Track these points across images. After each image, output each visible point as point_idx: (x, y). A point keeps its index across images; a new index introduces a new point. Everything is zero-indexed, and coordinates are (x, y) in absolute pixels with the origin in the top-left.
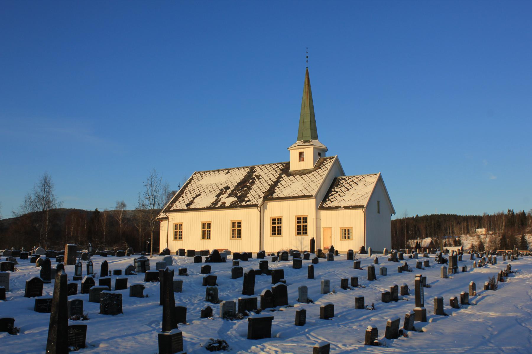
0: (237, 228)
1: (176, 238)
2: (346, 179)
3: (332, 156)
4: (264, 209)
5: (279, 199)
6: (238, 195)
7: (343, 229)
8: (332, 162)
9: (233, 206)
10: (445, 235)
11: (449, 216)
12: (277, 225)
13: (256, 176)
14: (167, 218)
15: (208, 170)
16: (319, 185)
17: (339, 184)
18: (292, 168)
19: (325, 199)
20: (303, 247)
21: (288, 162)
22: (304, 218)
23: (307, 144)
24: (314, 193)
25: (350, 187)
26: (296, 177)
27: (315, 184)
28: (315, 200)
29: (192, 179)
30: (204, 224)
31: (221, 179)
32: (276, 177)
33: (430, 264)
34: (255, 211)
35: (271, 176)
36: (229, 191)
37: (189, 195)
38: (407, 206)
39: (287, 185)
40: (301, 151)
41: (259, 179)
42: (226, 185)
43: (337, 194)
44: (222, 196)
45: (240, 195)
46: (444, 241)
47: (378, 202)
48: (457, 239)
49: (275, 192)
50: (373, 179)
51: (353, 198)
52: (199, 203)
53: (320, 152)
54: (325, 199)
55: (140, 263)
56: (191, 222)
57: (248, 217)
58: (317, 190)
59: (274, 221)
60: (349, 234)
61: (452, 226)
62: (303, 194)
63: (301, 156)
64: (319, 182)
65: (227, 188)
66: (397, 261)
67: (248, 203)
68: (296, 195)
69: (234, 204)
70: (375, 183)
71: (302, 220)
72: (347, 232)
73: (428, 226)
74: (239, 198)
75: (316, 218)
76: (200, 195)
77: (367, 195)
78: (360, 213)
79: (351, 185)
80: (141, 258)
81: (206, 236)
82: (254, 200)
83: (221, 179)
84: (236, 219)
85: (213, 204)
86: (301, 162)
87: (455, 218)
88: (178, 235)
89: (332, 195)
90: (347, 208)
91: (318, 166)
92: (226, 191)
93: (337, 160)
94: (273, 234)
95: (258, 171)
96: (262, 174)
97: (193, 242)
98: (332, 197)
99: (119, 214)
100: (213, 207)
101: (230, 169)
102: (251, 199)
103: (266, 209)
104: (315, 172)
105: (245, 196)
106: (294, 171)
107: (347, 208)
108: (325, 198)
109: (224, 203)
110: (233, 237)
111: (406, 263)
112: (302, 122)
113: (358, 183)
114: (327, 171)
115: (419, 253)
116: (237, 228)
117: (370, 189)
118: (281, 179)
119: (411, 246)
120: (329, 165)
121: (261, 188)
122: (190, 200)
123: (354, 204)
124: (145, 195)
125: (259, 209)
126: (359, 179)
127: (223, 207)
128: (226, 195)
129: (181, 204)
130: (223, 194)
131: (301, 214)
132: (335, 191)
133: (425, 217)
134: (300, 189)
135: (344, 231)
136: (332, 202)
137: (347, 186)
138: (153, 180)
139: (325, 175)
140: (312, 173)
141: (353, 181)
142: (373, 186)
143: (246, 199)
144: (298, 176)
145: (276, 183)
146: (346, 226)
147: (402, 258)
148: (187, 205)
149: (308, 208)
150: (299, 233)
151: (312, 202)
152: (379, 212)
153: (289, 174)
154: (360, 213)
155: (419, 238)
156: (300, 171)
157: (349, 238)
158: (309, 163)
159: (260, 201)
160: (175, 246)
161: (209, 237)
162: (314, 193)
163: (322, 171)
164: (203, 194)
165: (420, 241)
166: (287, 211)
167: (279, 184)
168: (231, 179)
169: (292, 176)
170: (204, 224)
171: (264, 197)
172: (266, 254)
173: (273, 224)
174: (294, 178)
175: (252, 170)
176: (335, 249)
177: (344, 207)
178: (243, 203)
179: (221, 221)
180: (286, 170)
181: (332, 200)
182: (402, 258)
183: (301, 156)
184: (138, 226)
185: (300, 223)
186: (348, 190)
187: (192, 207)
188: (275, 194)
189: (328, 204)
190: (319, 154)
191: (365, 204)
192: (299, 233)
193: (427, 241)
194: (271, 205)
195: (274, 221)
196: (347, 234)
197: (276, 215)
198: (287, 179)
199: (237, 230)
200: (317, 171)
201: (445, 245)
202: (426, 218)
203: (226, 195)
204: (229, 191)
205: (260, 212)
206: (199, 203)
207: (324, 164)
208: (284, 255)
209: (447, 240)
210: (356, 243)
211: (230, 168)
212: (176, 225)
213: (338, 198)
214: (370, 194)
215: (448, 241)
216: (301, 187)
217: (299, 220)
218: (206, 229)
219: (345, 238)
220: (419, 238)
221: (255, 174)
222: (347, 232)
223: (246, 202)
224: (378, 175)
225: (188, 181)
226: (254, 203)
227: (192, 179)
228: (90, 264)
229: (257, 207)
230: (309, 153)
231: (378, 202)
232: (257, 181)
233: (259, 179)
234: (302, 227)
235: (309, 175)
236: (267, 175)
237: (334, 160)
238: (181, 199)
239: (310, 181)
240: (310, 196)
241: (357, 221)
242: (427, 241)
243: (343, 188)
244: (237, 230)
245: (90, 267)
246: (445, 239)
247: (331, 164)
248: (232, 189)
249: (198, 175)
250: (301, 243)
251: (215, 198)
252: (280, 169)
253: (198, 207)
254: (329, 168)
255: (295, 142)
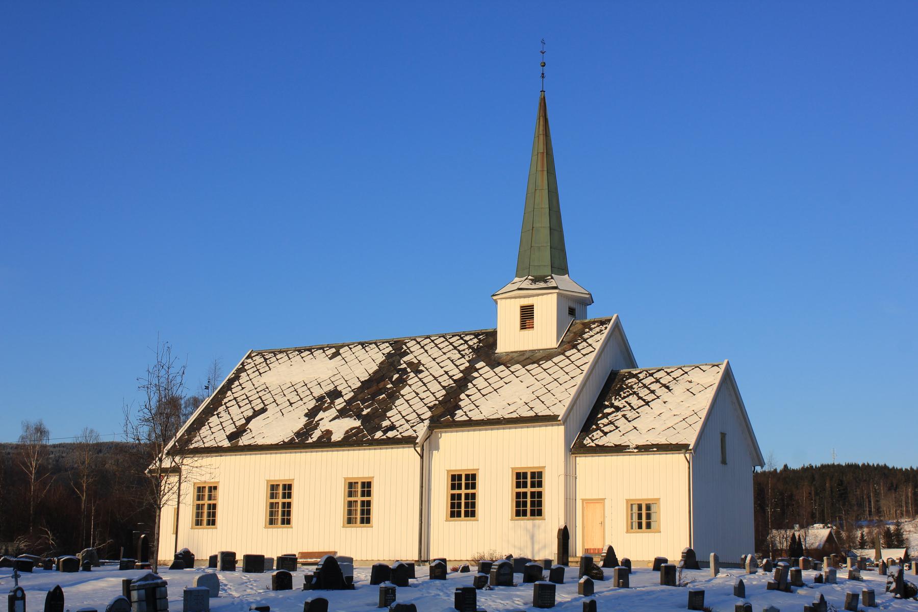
0: (359, 499)
1: (198, 523)
2: (641, 376)
3: (604, 317)
4: (430, 451)
5: (471, 424)
6: (365, 413)
7: (637, 501)
8: (606, 332)
9: (351, 441)
10: (858, 519)
11: (866, 468)
12: (463, 491)
13: (410, 364)
14: (176, 470)
15: (282, 347)
16: (573, 391)
17: (622, 389)
18: (503, 346)
19: (586, 428)
20: (536, 547)
21: (490, 329)
22: (533, 474)
23: (542, 285)
24: (560, 411)
25: (652, 396)
26: (512, 369)
27: (562, 388)
28: (562, 428)
29: (242, 369)
30: (274, 487)
31: (318, 371)
32: (462, 368)
33: (878, 601)
34: (408, 454)
35: (450, 366)
36: (340, 403)
37: (234, 410)
38: (787, 446)
39: (490, 389)
40: (526, 302)
41: (417, 372)
42: (331, 387)
43: (620, 414)
44: (321, 415)
45: (369, 411)
46: (859, 534)
47: (723, 435)
48: (892, 528)
49: (460, 408)
50: (712, 378)
51: (659, 425)
52: (264, 431)
53: (573, 305)
54: (586, 428)
55: (143, 592)
56: (242, 484)
57: (390, 470)
58: (567, 402)
59: (455, 480)
60: (649, 516)
61: (877, 494)
62: (531, 414)
63: (528, 318)
64: (572, 382)
65: (335, 394)
66: (787, 589)
67: (390, 434)
68: (514, 415)
69: (355, 435)
70: (715, 387)
71: (529, 480)
72: (644, 512)
73: (817, 494)
74: (365, 420)
75: (566, 475)
76: (263, 410)
77: (695, 418)
78: (679, 464)
79: (653, 392)
80: (145, 578)
81: (280, 517)
82: (407, 426)
83: (318, 371)
84: (360, 474)
85: (298, 434)
86: (526, 332)
87: (884, 472)
88: (206, 515)
89: (606, 416)
90: (644, 449)
91: (571, 339)
92: (332, 402)
93: (617, 327)
94: (452, 515)
95: (415, 353)
96: (424, 359)
97: (242, 529)
98: (605, 421)
99: (28, 456)
100: (299, 442)
101: (342, 346)
102: (397, 424)
103: (437, 449)
104: (562, 357)
105: (384, 417)
106: (507, 354)
107: (644, 449)
108: (589, 424)
109: (328, 433)
110: (350, 521)
111: (822, 597)
112: (529, 230)
113: (671, 386)
114: (594, 354)
115: (806, 568)
116: (359, 499)
117: (704, 401)
118: (475, 374)
119: (779, 546)
120: (597, 339)
121: (422, 395)
122: (238, 424)
123: (662, 441)
124: (141, 414)
125: (419, 449)
126: (674, 375)
127: (326, 442)
128: (333, 412)
129: (215, 433)
130: (325, 410)
131: (528, 463)
132: (612, 405)
133: (805, 470)
134: (524, 400)
135: (635, 508)
136: (605, 434)
137: (643, 393)
138: (163, 372)
139: (588, 366)
140: (556, 360)
141: (657, 381)
142: (710, 394)
143: (385, 423)
144: (518, 366)
145: (463, 383)
146: (643, 494)
147: (798, 582)
148: (232, 437)
149: (545, 447)
150: (520, 512)
151: (555, 435)
152: (724, 462)
153: (494, 362)
154: (679, 464)
155: (797, 527)
156: (523, 353)
157: (649, 526)
158: (545, 333)
159: (422, 430)
160: (206, 544)
161: (287, 521)
162: (560, 411)
163: (579, 355)
164: (272, 409)
165: (802, 532)
166: (493, 458)
167: (470, 385)
168: (345, 370)
169: (502, 367)
170: (274, 487)
171: (432, 419)
172: (449, 567)
173: (453, 487)
174: (507, 372)
175: (399, 348)
176: (620, 557)
177: (637, 447)
178: (378, 435)
179: (321, 478)
180: (485, 349)
181: (606, 429)
182: (798, 582)
183: (527, 316)
184: (80, 487)
185: (525, 486)
186: (647, 403)
187: (244, 441)
188: (459, 413)
189: (597, 438)
190: (572, 312)
191: (690, 437)
192: (520, 512)
193: (818, 534)
194: (448, 439)
195: (455, 480)
196: (643, 516)
197: (463, 466)
198: (491, 373)
199: (359, 504)
200: (568, 354)
201: (863, 545)
202: (809, 472)
203: (333, 412)
204: (340, 403)
205: (422, 457)
206: (264, 431)
207: (586, 336)
208: (502, 571)
209: (866, 530)
210: (672, 539)
211: (340, 342)
212: (200, 490)
213: (621, 423)
214: (703, 414)
215: (870, 533)
216: (527, 396)
217: (520, 478)
218: (280, 500)
219: (640, 526)
220: (797, 527)
221: (406, 359)
222: (644, 512)
223: (385, 432)
224: (723, 367)
225: (230, 375)
226: (405, 434)
227: (242, 369)
228: (19, 594)
229: (415, 444)
230: (547, 307)
231: (723, 435)
232: (412, 379)
233: (417, 372)
234: (528, 498)
235: (546, 365)
236: (438, 364)
237: (609, 326)
238: (214, 420)
239: (550, 379)
240: (551, 419)
241: (669, 483)
242: (818, 534)
243: (633, 400)
244: (359, 504)
245: (18, 603)
246: (861, 527)
247: (602, 337)
248: (347, 397)
249: (259, 360)
250: (532, 537)
251: (304, 420)
252: (470, 347)
253: (260, 442)
254: (598, 346)
255: (510, 282)
